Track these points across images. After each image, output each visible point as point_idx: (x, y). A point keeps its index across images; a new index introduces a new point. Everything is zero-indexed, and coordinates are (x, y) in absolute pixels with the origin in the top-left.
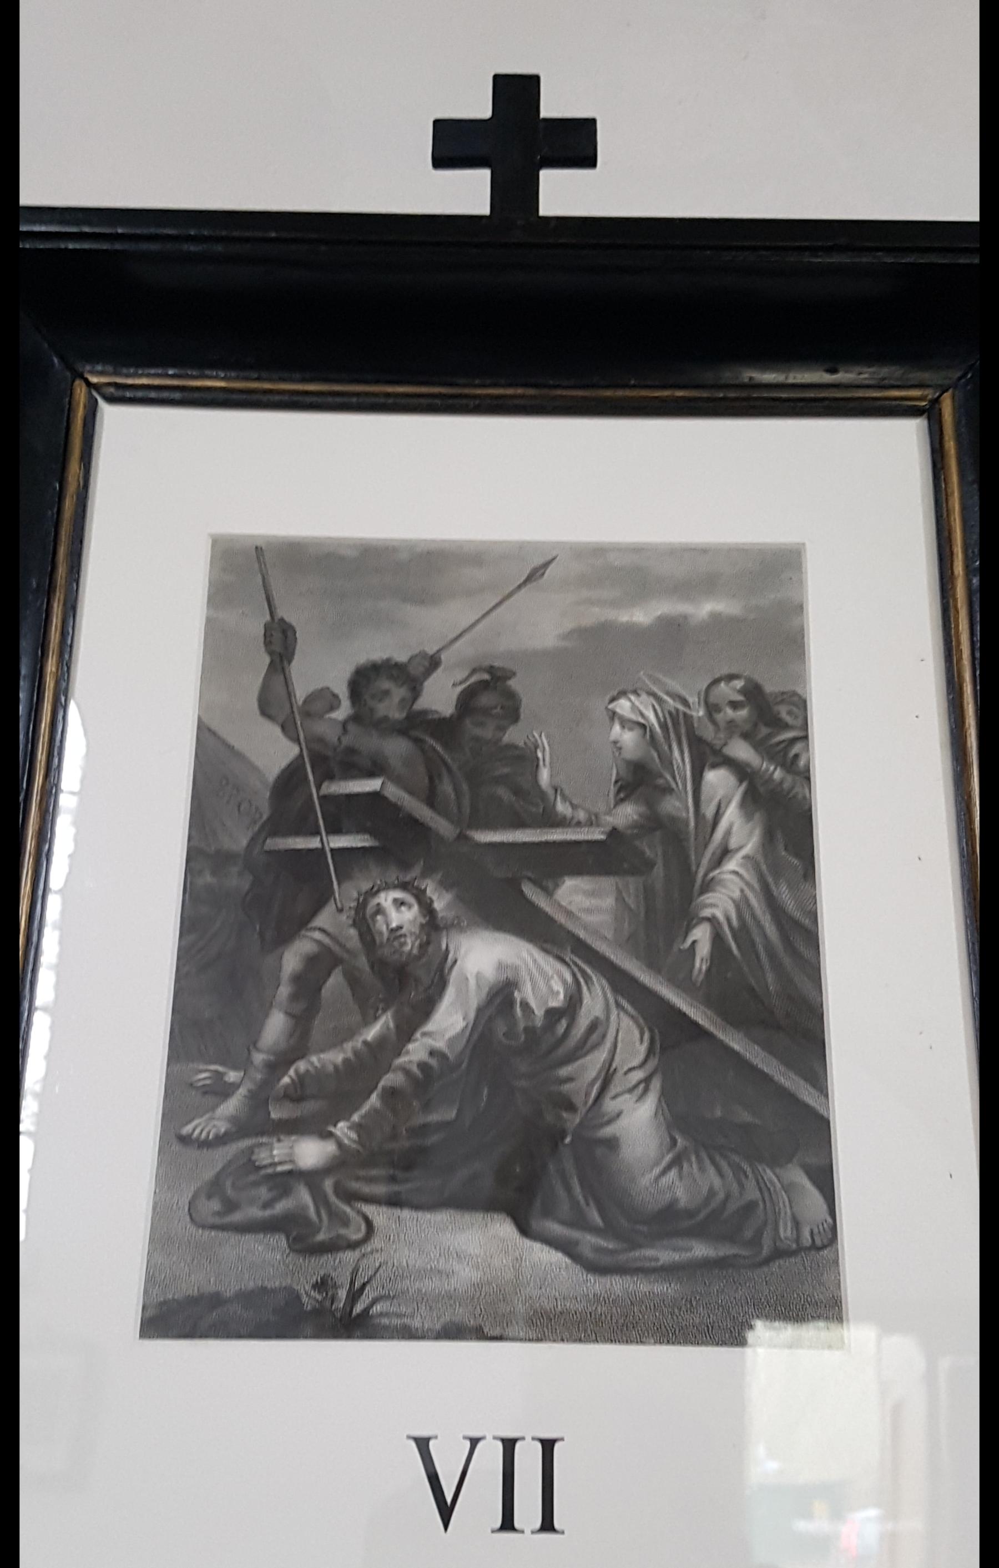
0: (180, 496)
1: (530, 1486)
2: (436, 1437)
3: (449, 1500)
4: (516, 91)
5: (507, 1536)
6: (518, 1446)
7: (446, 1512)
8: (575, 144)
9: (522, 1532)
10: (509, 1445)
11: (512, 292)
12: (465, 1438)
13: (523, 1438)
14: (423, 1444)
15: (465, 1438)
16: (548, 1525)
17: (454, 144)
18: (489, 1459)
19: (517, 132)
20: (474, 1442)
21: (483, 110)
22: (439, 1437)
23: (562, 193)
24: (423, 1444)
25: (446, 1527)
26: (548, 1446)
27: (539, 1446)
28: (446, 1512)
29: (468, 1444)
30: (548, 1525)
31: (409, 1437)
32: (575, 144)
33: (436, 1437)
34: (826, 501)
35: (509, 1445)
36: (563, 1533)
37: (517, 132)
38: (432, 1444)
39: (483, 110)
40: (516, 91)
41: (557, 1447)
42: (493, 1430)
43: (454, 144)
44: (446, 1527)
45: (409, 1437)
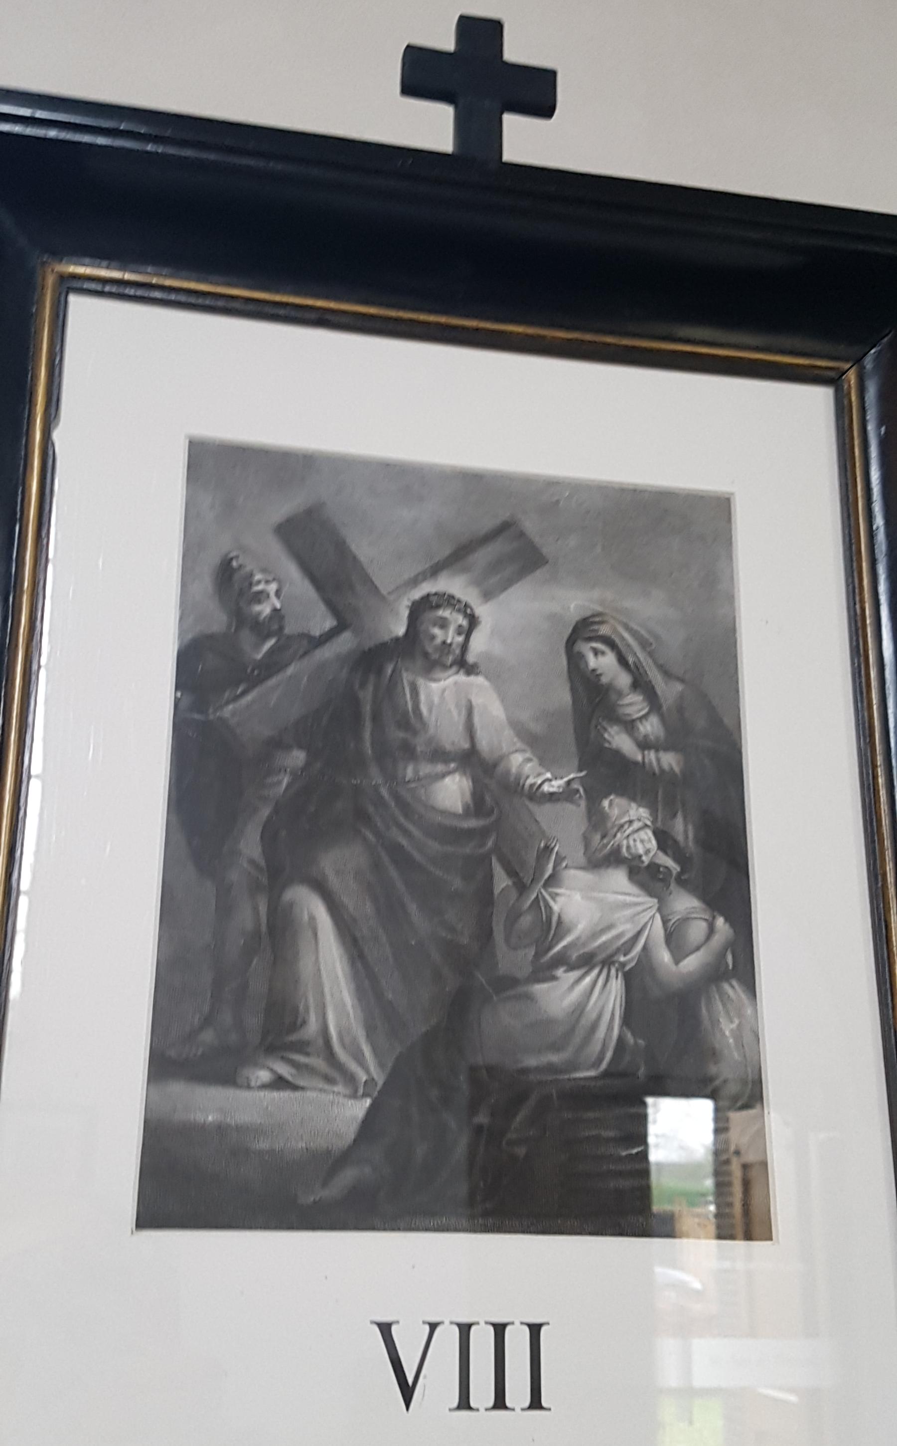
0: (149, 388)
1: (508, 1365)
2: (398, 1322)
3: (410, 1380)
4: (482, 34)
5: (464, 1413)
6: (508, 1329)
7: (407, 1392)
8: (535, 92)
9: (513, 1410)
10: (465, 1329)
11: (461, 231)
12: (424, 1323)
13: (513, 1323)
14: (385, 1329)
15: (424, 1323)
16: (536, 1403)
17: (423, 74)
18: (447, 1341)
19: (476, 73)
20: (433, 1327)
21: (448, 43)
22: (401, 1323)
23: (524, 141)
24: (385, 1329)
25: (408, 1407)
26: (535, 1330)
27: (527, 1330)
28: (407, 1392)
29: (427, 1328)
30: (536, 1403)
31: (373, 1322)
32: (535, 92)
33: (398, 1322)
34: (754, 445)
35: (465, 1329)
36: (549, 1409)
37: (476, 73)
38: (394, 1329)
39: (448, 43)
40: (482, 34)
41: (543, 1330)
42: (451, 1314)
43: (423, 74)
44: (408, 1407)
45: (373, 1322)
